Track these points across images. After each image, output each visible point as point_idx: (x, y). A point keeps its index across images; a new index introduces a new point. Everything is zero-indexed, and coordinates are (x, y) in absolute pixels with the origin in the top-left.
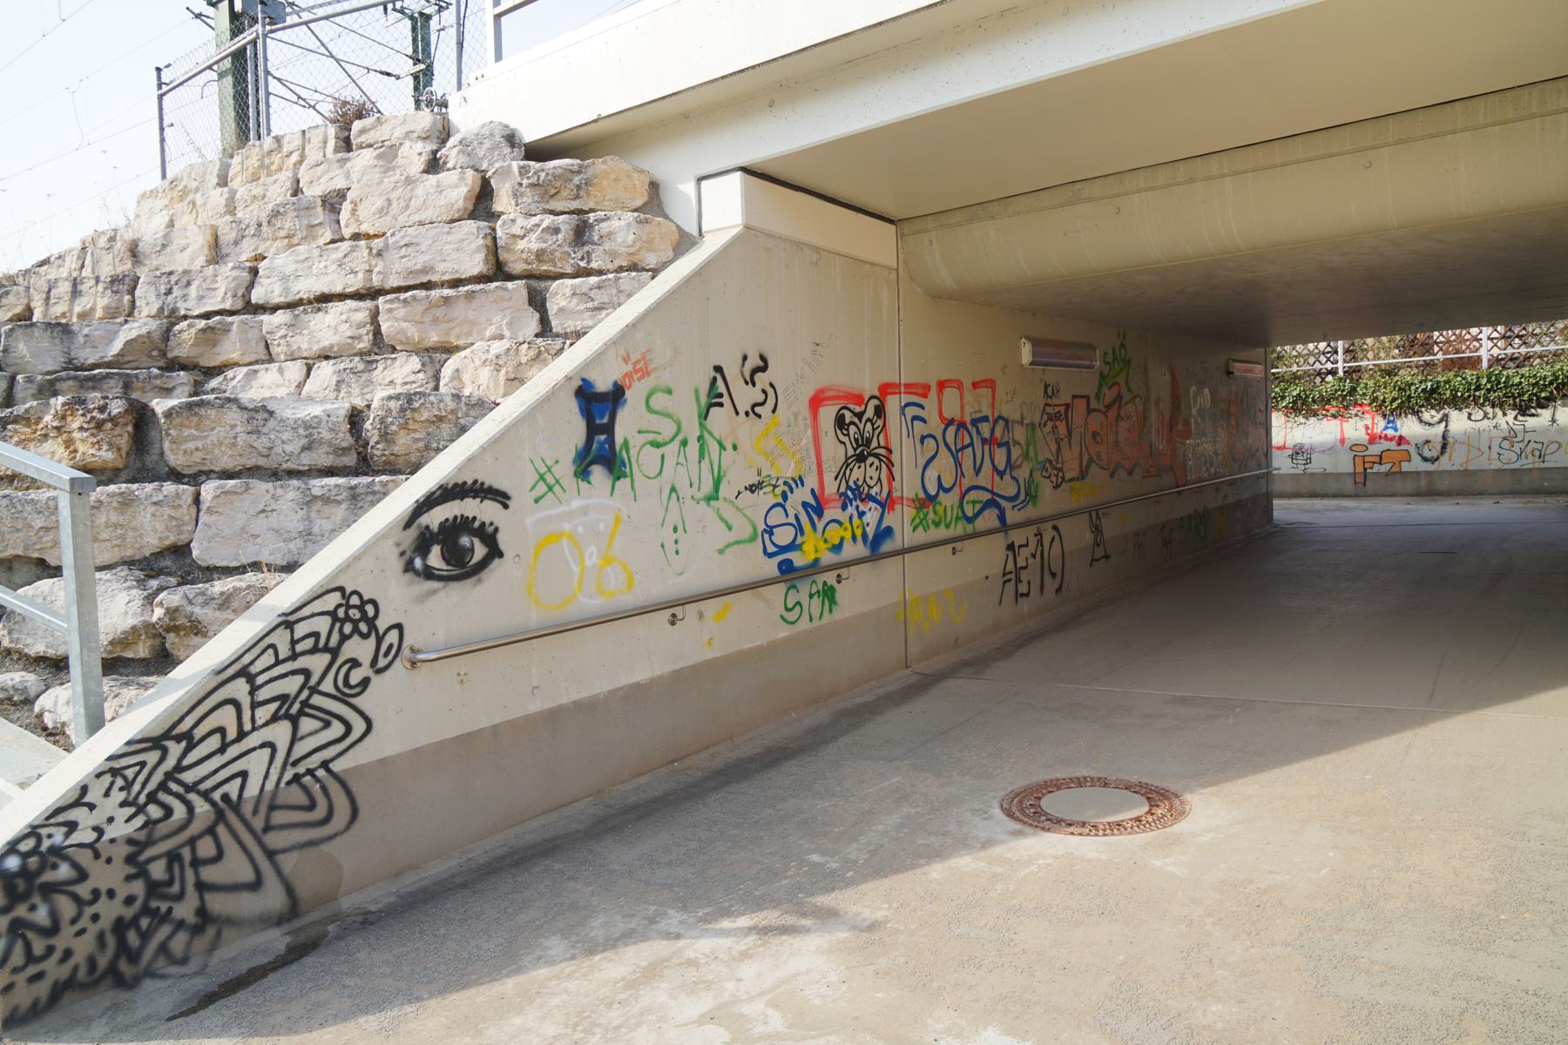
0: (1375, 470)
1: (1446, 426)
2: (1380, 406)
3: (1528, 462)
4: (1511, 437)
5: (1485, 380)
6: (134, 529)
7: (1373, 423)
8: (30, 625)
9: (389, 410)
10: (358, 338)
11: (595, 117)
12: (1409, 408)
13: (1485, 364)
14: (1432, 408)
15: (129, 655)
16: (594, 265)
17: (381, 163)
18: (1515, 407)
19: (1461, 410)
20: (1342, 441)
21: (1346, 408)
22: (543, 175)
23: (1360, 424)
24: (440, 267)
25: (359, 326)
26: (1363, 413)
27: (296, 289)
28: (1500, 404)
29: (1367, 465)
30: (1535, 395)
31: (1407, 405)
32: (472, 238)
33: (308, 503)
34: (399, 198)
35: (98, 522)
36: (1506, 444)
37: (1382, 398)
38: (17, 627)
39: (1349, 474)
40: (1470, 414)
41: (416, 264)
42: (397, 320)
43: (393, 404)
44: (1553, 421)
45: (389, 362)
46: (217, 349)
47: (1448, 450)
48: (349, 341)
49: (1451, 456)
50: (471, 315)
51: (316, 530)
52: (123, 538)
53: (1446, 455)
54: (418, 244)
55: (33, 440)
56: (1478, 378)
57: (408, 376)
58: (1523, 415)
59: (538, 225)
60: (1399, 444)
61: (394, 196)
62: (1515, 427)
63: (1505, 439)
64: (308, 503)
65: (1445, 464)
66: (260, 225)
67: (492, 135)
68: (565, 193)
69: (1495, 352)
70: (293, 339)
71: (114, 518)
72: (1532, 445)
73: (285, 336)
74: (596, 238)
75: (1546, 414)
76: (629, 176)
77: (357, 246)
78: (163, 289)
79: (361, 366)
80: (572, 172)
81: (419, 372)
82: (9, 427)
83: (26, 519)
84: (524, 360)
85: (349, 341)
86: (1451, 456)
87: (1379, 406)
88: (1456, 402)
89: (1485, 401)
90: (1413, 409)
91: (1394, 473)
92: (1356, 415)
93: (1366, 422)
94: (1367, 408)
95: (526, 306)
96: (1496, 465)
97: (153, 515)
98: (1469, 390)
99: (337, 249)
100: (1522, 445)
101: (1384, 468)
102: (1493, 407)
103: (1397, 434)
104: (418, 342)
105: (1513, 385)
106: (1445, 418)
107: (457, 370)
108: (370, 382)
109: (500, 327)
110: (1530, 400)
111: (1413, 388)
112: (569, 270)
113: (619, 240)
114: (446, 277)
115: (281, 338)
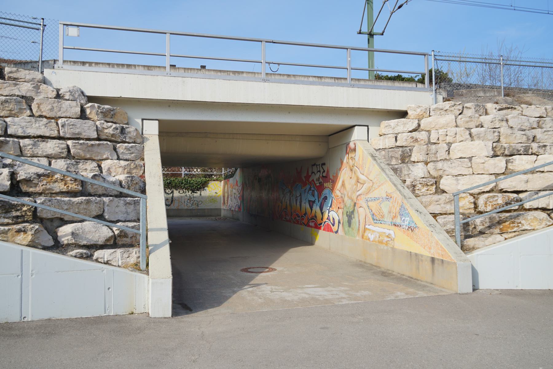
3: (194, 207)
4: (190, 199)
5: (184, 181)
6: (89, 210)
8: (80, 236)
9: (128, 180)
11: (119, 96)
13: (183, 176)
15: (108, 243)
16: (127, 140)
17: (35, 90)
19: (177, 190)
22: (104, 110)
24: (84, 134)
25: (63, 149)
27: (28, 132)
28: (187, 189)
30: (197, 186)
32: (92, 126)
33: (126, 204)
34: (57, 107)
35: (80, 207)
36: (189, 201)
38: (76, 237)
40: (179, 191)
41: (76, 131)
42: (77, 149)
43: (128, 178)
44: (201, 195)
45: (85, 163)
47: (173, 202)
48: (59, 153)
50: (99, 151)
51: (128, 211)
52: (86, 212)
53: (173, 204)
54: (76, 125)
55: (51, 182)
57: (92, 168)
59: (111, 126)
61: (55, 105)
62: (191, 196)
63: (188, 199)
64: (126, 204)
67: (77, 91)
68: (109, 116)
69: (186, 172)
70: (35, 150)
71: (85, 207)
72: (195, 202)
73: (32, 148)
74: (126, 133)
75: (199, 192)
76: (124, 114)
77: (51, 121)
79: (75, 163)
80: (111, 110)
81: (96, 167)
82: (42, 177)
83: (62, 206)
84: (132, 167)
85: (59, 153)
95: (113, 150)
96: (186, 207)
97: (95, 206)
98: (180, 184)
99: (42, 120)
100: (193, 202)
102: (186, 189)
104: (83, 157)
106: (172, 192)
107: (109, 168)
109: (108, 155)
110: (195, 188)
112: (119, 140)
113: (132, 134)
114: (85, 137)
115: (30, 149)
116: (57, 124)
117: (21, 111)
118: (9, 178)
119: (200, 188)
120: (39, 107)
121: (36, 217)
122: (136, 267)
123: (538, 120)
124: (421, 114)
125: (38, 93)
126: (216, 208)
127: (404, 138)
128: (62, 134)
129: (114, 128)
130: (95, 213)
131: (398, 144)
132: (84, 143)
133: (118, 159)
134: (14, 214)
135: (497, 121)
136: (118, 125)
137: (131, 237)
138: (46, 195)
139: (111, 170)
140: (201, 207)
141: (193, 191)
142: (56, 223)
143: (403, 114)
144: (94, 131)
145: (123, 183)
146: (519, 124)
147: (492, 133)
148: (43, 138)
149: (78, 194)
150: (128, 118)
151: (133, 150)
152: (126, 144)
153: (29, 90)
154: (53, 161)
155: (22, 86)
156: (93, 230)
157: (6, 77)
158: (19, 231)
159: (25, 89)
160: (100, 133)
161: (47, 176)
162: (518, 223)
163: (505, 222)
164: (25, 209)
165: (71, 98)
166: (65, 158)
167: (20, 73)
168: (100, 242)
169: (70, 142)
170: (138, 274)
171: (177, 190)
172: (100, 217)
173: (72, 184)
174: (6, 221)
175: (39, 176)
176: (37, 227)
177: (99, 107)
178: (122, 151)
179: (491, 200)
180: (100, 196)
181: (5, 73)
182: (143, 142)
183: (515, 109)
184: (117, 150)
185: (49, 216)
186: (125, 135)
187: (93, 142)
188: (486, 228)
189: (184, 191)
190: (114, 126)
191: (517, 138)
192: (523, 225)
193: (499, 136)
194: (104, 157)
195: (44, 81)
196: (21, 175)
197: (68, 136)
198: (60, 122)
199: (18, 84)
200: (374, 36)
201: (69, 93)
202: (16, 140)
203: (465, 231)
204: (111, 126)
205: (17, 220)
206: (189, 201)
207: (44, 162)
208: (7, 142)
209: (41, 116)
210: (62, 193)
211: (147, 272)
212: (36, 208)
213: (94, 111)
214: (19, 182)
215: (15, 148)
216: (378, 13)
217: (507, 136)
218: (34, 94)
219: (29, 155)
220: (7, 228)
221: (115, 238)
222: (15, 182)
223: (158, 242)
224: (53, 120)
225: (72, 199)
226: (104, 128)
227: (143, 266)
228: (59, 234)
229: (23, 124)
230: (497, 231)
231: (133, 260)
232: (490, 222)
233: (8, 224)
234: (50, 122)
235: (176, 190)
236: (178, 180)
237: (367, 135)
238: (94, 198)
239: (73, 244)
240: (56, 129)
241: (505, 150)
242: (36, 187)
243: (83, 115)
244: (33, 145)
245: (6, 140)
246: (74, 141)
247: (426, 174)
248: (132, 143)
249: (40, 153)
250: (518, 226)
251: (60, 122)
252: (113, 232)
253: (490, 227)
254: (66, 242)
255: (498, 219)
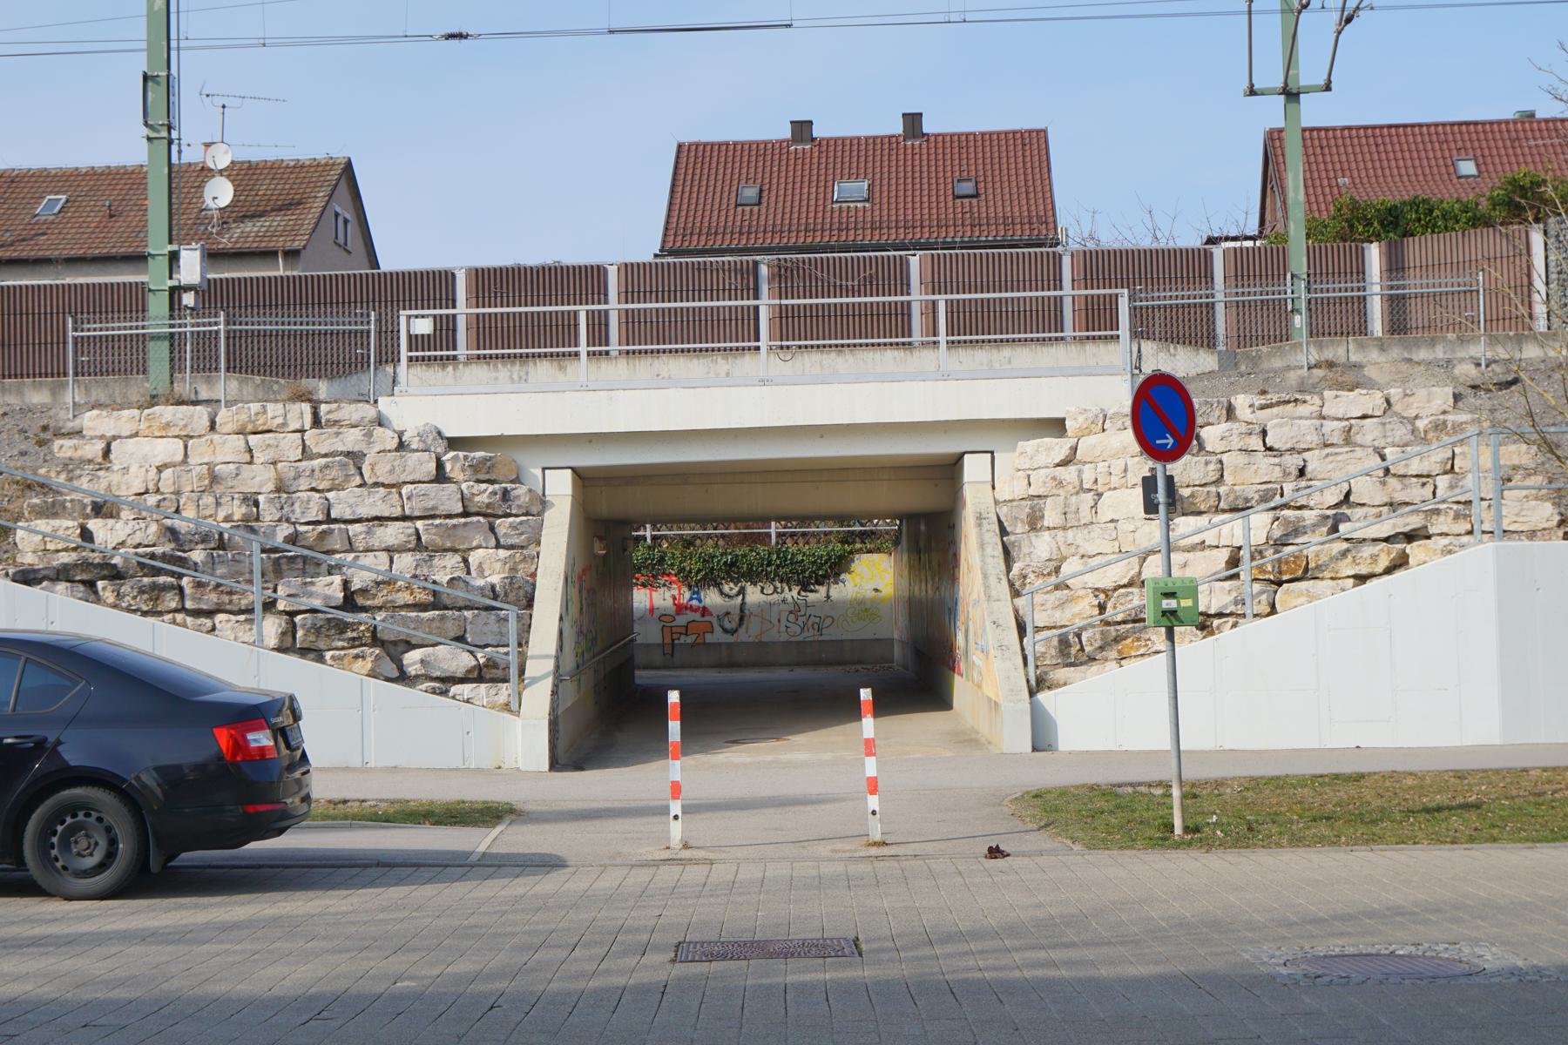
0: (682, 641)
1: (743, 599)
2: (687, 577)
3: (809, 635)
4: (796, 609)
5: (775, 557)
7: (680, 594)
10: (409, 542)
12: (712, 580)
14: (731, 581)
16: (514, 512)
18: (799, 583)
19: (755, 585)
20: (652, 610)
21: (654, 577)
23: (668, 595)
24: (442, 508)
25: (409, 536)
26: (671, 583)
28: (785, 580)
29: (675, 636)
31: (711, 579)
36: (792, 618)
37: (688, 569)
39: (659, 645)
40: (763, 588)
44: (828, 597)
46: (325, 542)
47: (745, 622)
49: (747, 628)
50: (465, 534)
56: (769, 554)
58: (805, 591)
59: (486, 490)
60: (703, 615)
61: (396, 463)
63: (791, 612)
65: (742, 636)
66: (313, 471)
67: (431, 432)
68: (484, 471)
71: (438, 624)
75: (822, 590)
78: (278, 506)
79: (427, 558)
86: (747, 628)
87: (685, 577)
88: (753, 576)
89: (775, 576)
90: (715, 581)
91: (699, 644)
92: (664, 585)
93: (673, 592)
94: (674, 578)
96: (784, 637)
98: (762, 565)
100: (804, 619)
101: (690, 639)
102: (781, 582)
103: (701, 605)
105: (797, 562)
106: (742, 591)
108: (431, 566)
110: (810, 577)
111: (716, 560)
112: (500, 513)
116: (400, 495)
117: (347, 477)
118: (341, 588)
119: (826, 577)
120: (372, 469)
121: (376, 640)
122: (506, 707)
123: (1345, 427)
124: (1085, 426)
125: (370, 443)
126: (876, 637)
127: (1041, 480)
128: (407, 512)
129: (491, 493)
130: (452, 634)
131: (1032, 491)
132: (441, 524)
133: (498, 546)
134: (350, 634)
135: (1234, 436)
136: (497, 486)
137: (504, 669)
138: (387, 609)
139: (484, 566)
140: (830, 634)
141: (805, 587)
142: (401, 647)
143: (1056, 426)
144: (457, 501)
145: (498, 589)
146: (1292, 438)
147: (1202, 465)
148: (380, 519)
149: (430, 608)
150: (518, 470)
151: (522, 529)
152: (511, 519)
153: (357, 441)
154: (396, 556)
155: (346, 435)
156: (450, 657)
157: (323, 421)
158: (357, 657)
159: (351, 439)
160: (466, 503)
161: (388, 583)
162: (1146, 640)
163: (1125, 638)
164: (362, 628)
165: (421, 446)
166: (413, 550)
167: (343, 411)
168: (459, 674)
169: (419, 524)
170: (507, 715)
171: (755, 584)
172: (460, 639)
173: (420, 593)
174: (340, 644)
175: (378, 583)
176: (377, 652)
177: (466, 458)
178: (504, 531)
179: (1123, 601)
180: (460, 609)
181: (322, 414)
182: (540, 514)
183: (1305, 402)
184: (496, 530)
185: (392, 638)
186: (510, 503)
187: (455, 521)
188: (1096, 649)
189: (775, 588)
190: (491, 488)
191: (1261, 472)
192: (1154, 643)
193: (1222, 469)
194: (474, 544)
195: (380, 422)
196: (356, 585)
197: (417, 513)
198: (404, 491)
199: (340, 433)
200: (1301, 95)
201: (418, 438)
202: (343, 526)
203: (1063, 655)
204: (486, 490)
205: (355, 642)
206: (792, 618)
207: (384, 556)
208: (331, 532)
209: (376, 484)
210: (407, 606)
211: (517, 713)
212: (375, 627)
213: (458, 465)
214: (353, 593)
215: (341, 539)
216: (1291, 41)
217: (1236, 470)
218: (364, 446)
219: (361, 549)
220: (342, 653)
221: (480, 670)
222: (348, 593)
223: (538, 674)
224: (394, 490)
225: (420, 614)
226: (473, 494)
227: (514, 706)
228: (405, 662)
229: (352, 501)
230: (1113, 654)
231: (502, 699)
232: (1102, 639)
233: (343, 648)
234: (390, 493)
235: (752, 583)
236: (758, 554)
237: (990, 471)
238: (450, 612)
239: (422, 675)
240: (399, 504)
241: (1219, 501)
242: (374, 598)
243: (441, 476)
244: (367, 533)
245: (329, 529)
246: (427, 522)
247: (1055, 552)
248: (523, 515)
249: (376, 544)
250: (1147, 645)
251: (405, 490)
252: (477, 660)
253: (1101, 648)
254: (413, 673)
255: (1114, 634)
